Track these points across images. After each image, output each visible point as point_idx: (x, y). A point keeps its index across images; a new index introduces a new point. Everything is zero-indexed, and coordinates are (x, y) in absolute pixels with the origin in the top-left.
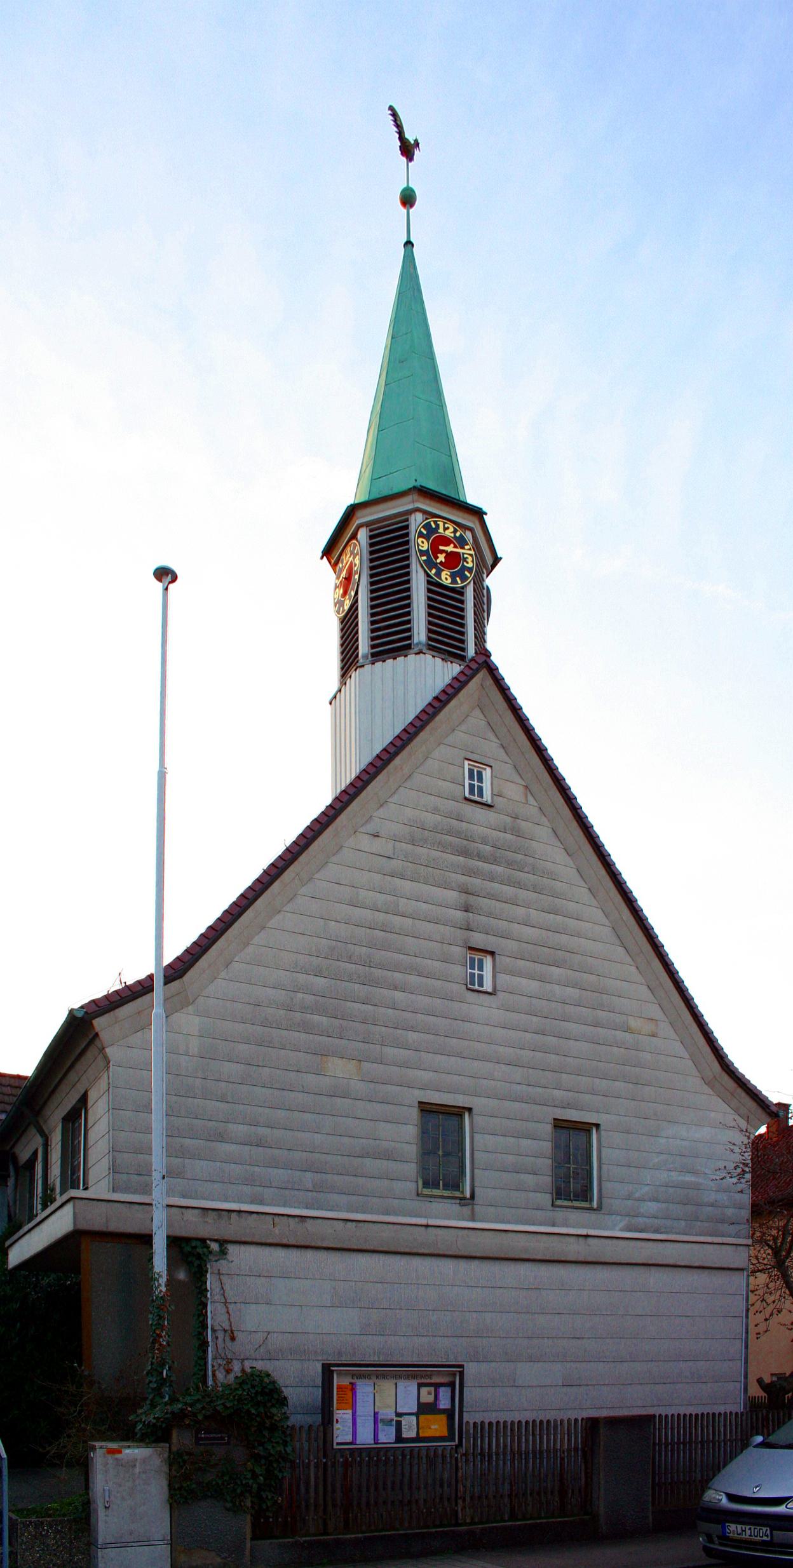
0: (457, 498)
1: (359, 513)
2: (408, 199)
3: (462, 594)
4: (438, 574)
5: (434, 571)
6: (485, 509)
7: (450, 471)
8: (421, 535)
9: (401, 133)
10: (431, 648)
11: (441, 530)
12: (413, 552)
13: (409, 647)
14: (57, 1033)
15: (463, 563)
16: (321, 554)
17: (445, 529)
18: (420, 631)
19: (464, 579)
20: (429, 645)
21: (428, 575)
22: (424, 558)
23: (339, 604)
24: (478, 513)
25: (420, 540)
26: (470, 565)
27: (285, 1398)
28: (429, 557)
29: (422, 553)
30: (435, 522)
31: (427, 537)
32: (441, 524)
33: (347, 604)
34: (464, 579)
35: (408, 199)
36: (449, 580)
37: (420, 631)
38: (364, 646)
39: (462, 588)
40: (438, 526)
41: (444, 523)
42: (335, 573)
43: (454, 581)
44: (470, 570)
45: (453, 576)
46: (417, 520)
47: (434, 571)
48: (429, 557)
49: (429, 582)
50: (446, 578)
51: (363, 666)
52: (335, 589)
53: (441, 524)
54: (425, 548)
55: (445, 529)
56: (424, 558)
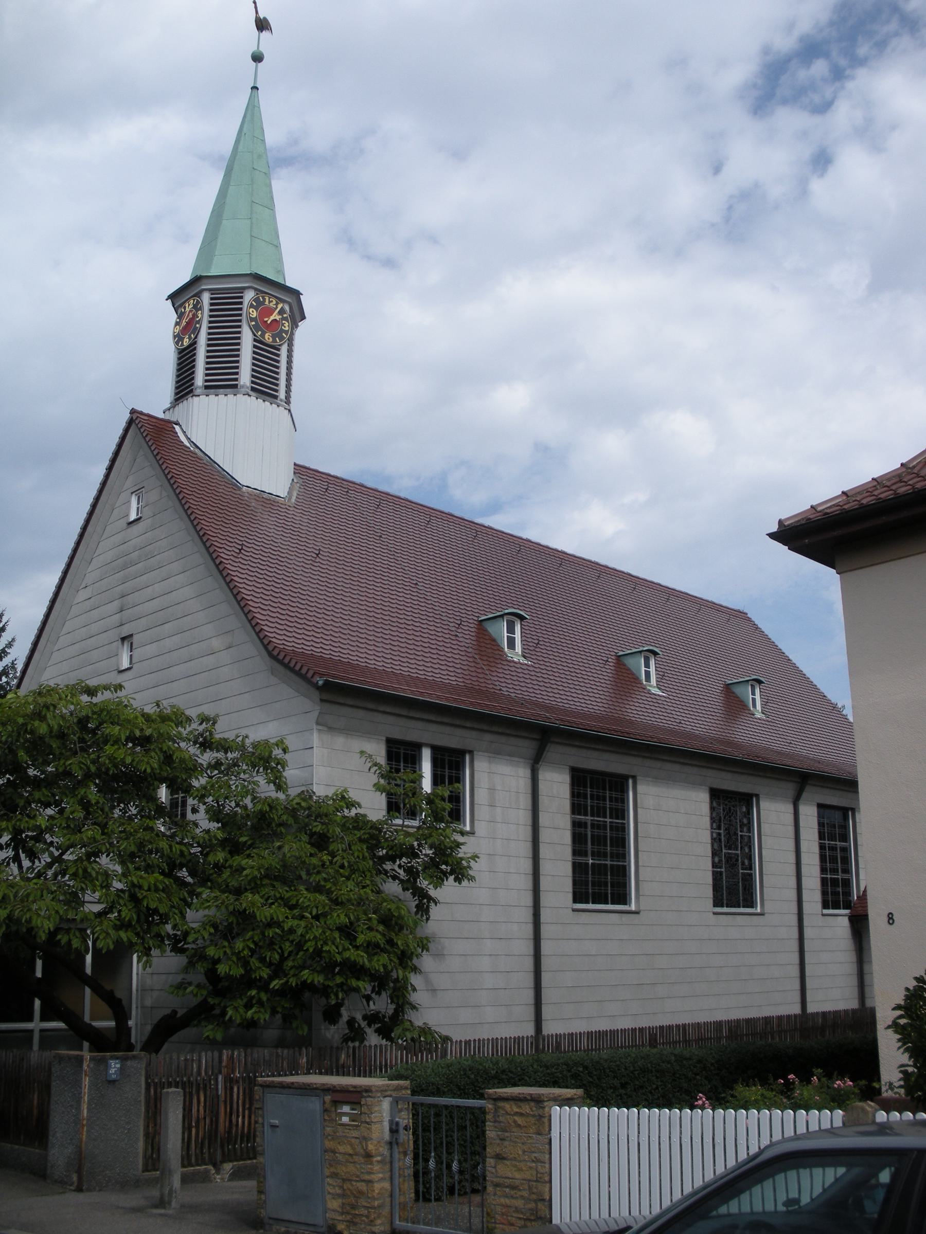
0: (283, 283)
1: (205, 281)
2: (257, 58)
3: (279, 350)
4: (263, 335)
5: (260, 333)
6: (301, 292)
7: (281, 272)
8: (252, 306)
9: (257, 12)
10: (253, 389)
11: (267, 303)
12: (244, 318)
13: (236, 386)
14: (869, 937)
15: (383, 1092)
16: (166, 297)
17: (270, 302)
18: (245, 377)
19: (282, 338)
20: (252, 387)
21: (255, 335)
22: (253, 323)
23: (178, 338)
24: (296, 294)
25: (251, 310)
26: (287, 329)
27: (902, 465)
28: (256, 322)
29: (252, 319)
30: (263, 297)
31: (256, 308)
32: (267, 299)
33: (186, 342)
34: (282, 338)
35: (257, 58)
36: (271, 339)
37: (245, 377)
38: (199, 379)
39: (280, 345)
40: (264, 300)
41: (269, 298)
42: (177, 313)
43: (274, 341)
44: (286, 332)
45: (274, 337)
46: (249, 296)
47: (260, 333)
48: (256, 322)
49: (255, 340)
50: (268, 338)
51: (199, 396)
52: (176, 326)
53: (267, 299)
54: (254, 316)
55: (270, 302)
56: (253, 323)
